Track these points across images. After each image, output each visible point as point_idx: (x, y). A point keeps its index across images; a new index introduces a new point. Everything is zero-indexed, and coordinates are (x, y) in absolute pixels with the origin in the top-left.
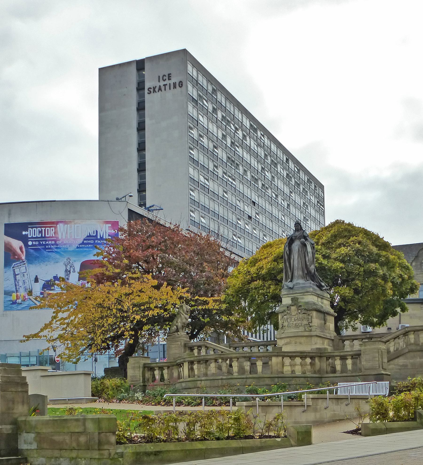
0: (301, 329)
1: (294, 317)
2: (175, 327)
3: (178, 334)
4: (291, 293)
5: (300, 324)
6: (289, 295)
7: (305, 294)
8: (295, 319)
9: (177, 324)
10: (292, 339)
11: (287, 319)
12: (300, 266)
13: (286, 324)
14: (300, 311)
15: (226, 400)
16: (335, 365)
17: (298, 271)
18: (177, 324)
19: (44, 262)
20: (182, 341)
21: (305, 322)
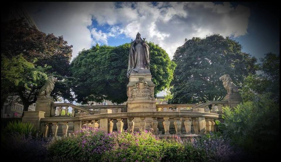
0: (147, 97)
1: (142, 90)
2: (44, 92)
3: (46, 97)
4: (137, 75)
5: (146, 95)
6: (136, 76)
7: (147, 76)
8: (142, 91)
9: (46, 90)
10: (141, 105)
11: (136, 91)
12: (142, 59)
13: (134, 94)
14: (145, 87)
15: (90, 160)
16: (174, 126)
17: (140, 62)
18: (46, 90)
19: (128, 145)
20: (50, 102)
21: (149, 94)
